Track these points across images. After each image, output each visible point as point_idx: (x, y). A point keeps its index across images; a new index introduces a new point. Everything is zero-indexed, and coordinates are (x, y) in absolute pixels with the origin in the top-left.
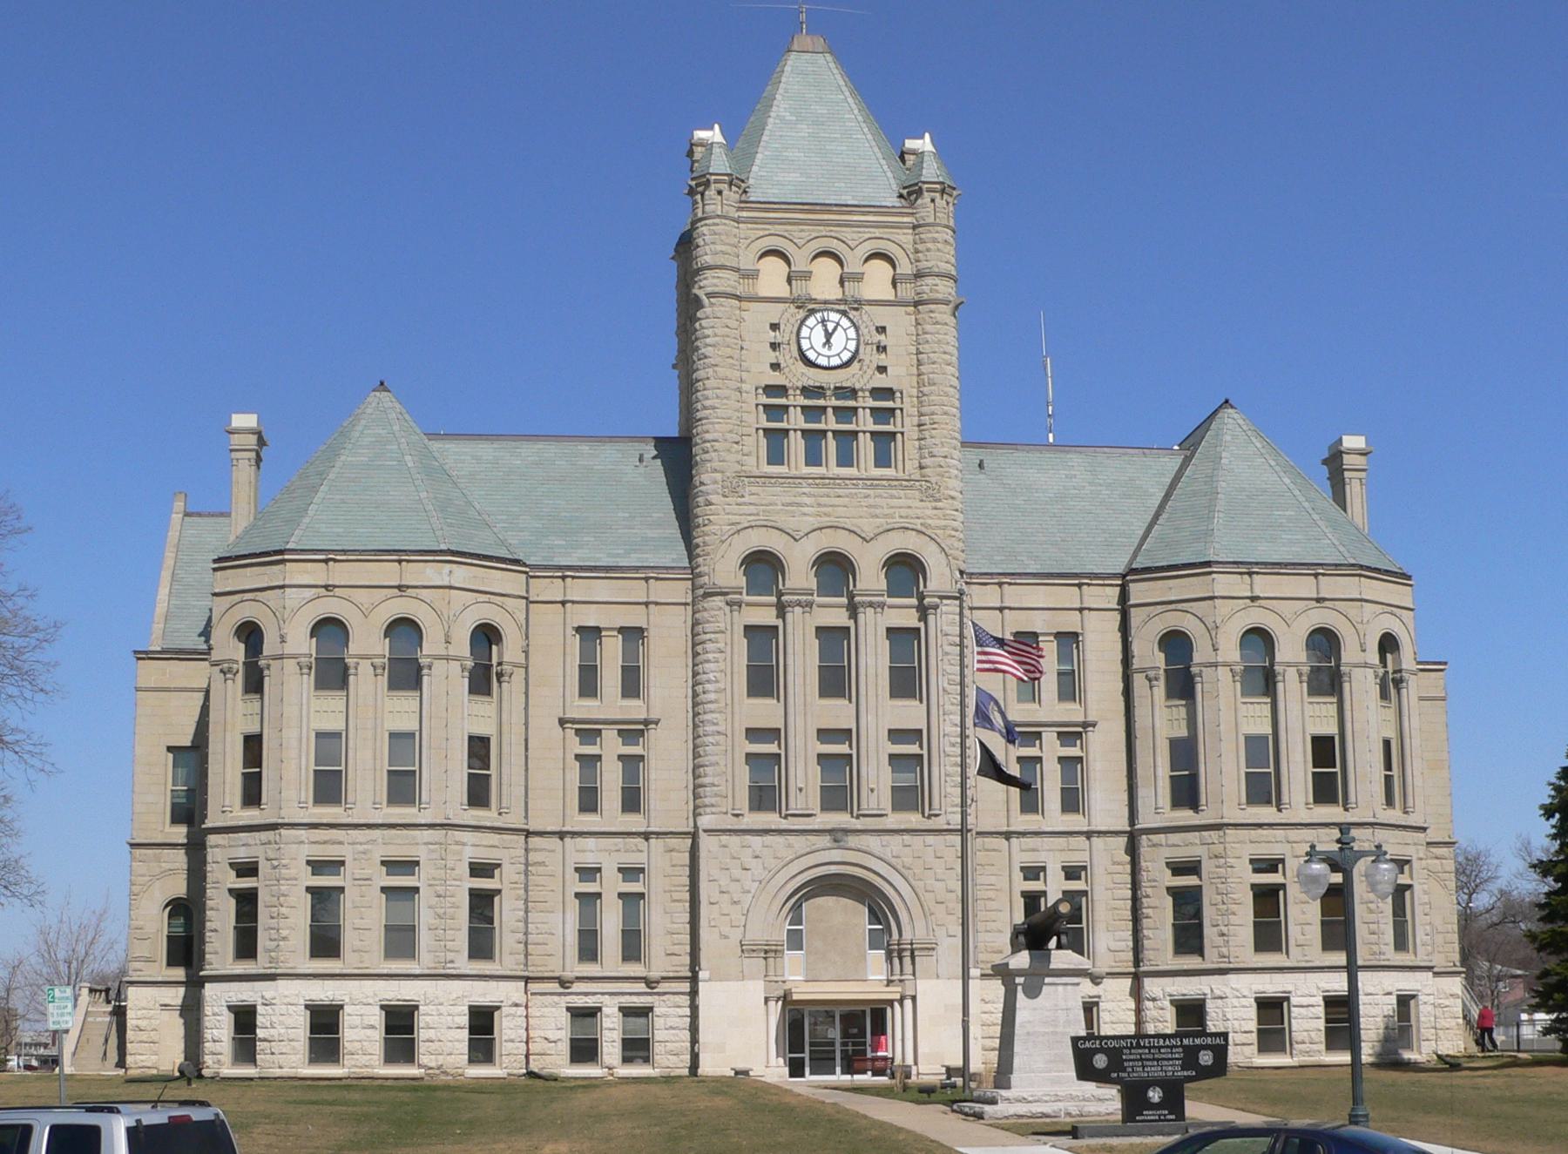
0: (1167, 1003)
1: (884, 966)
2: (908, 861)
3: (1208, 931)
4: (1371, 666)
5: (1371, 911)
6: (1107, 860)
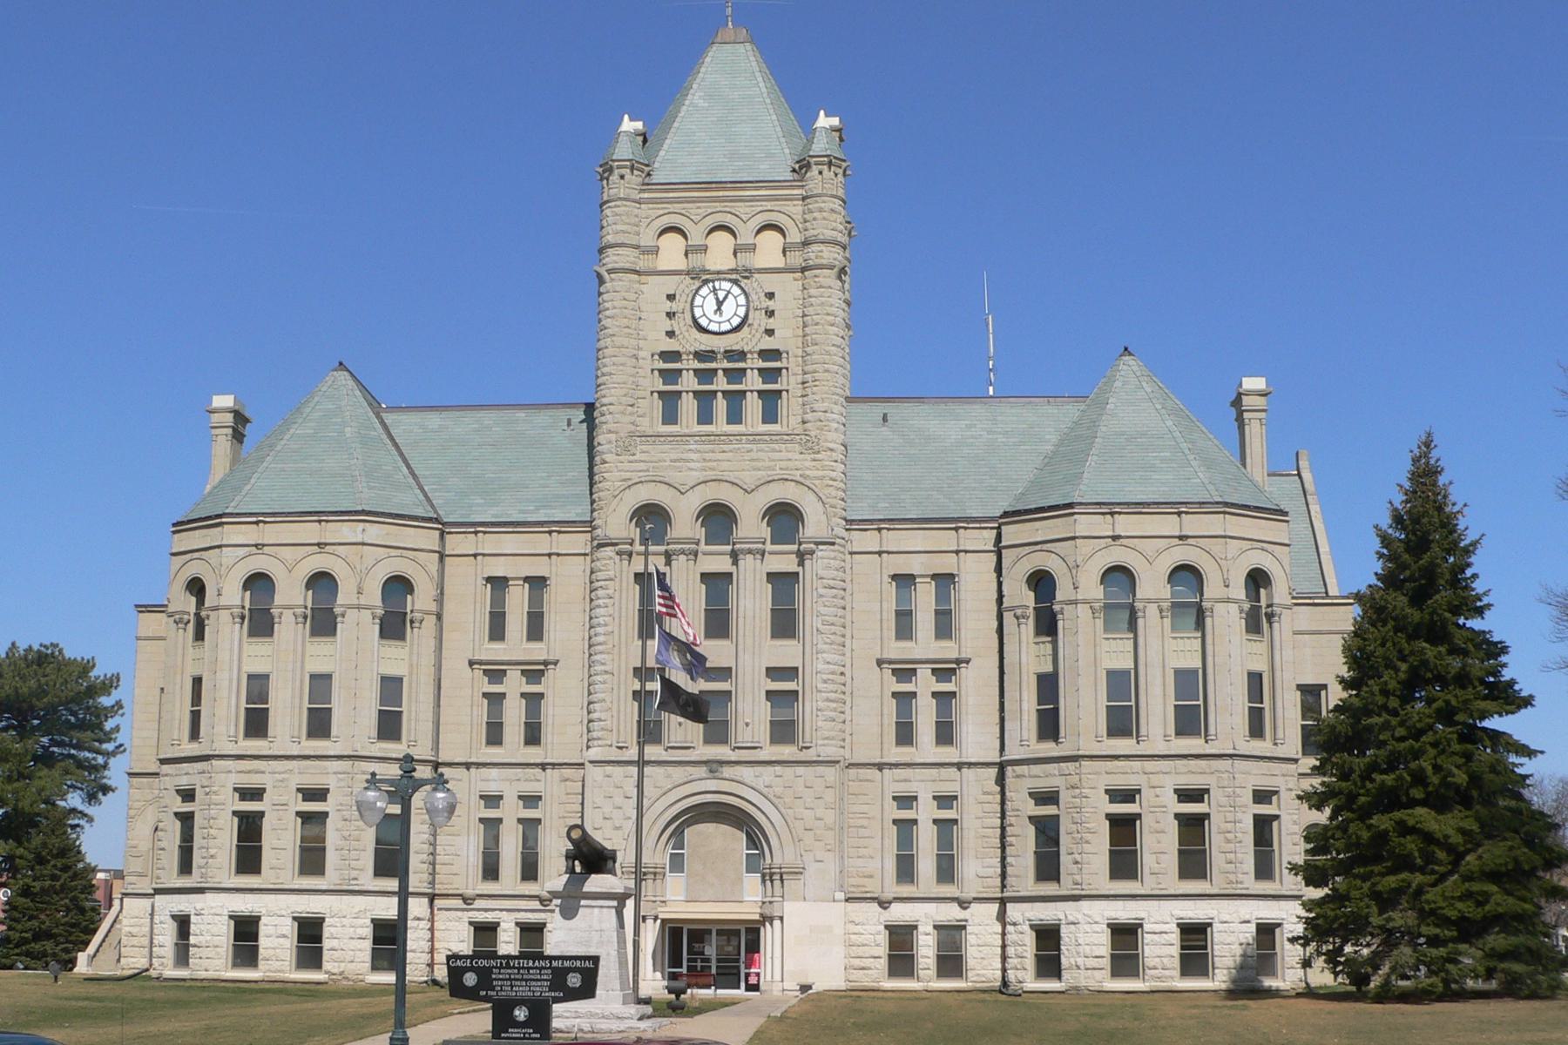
0: (1026, 928)
1: (760, 887)
2: (778, 790)
3: (1065, 860)
4: (1235, 601)
5: (1228, 841)
6: (977, 789)
